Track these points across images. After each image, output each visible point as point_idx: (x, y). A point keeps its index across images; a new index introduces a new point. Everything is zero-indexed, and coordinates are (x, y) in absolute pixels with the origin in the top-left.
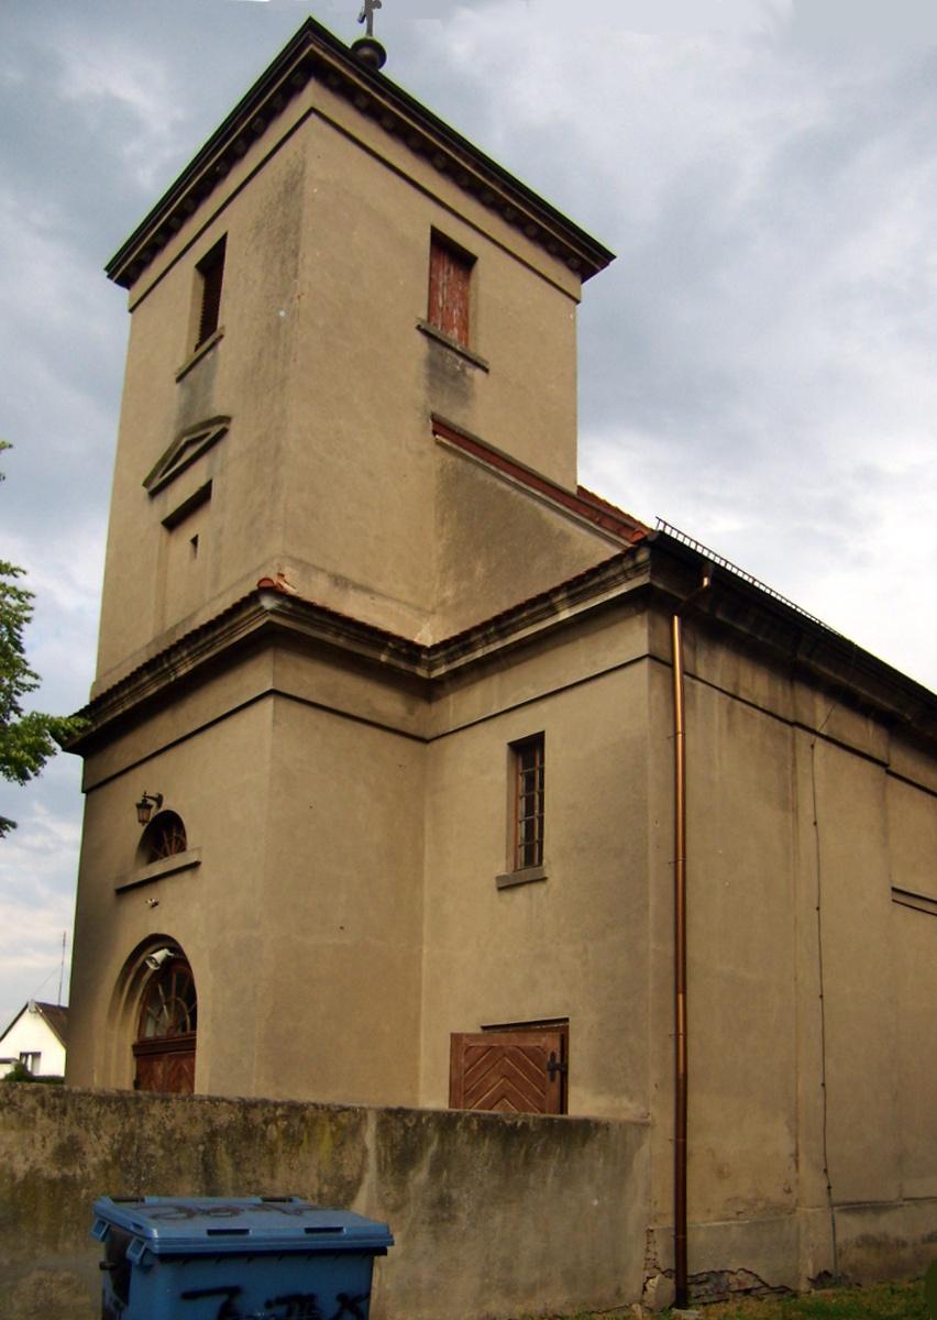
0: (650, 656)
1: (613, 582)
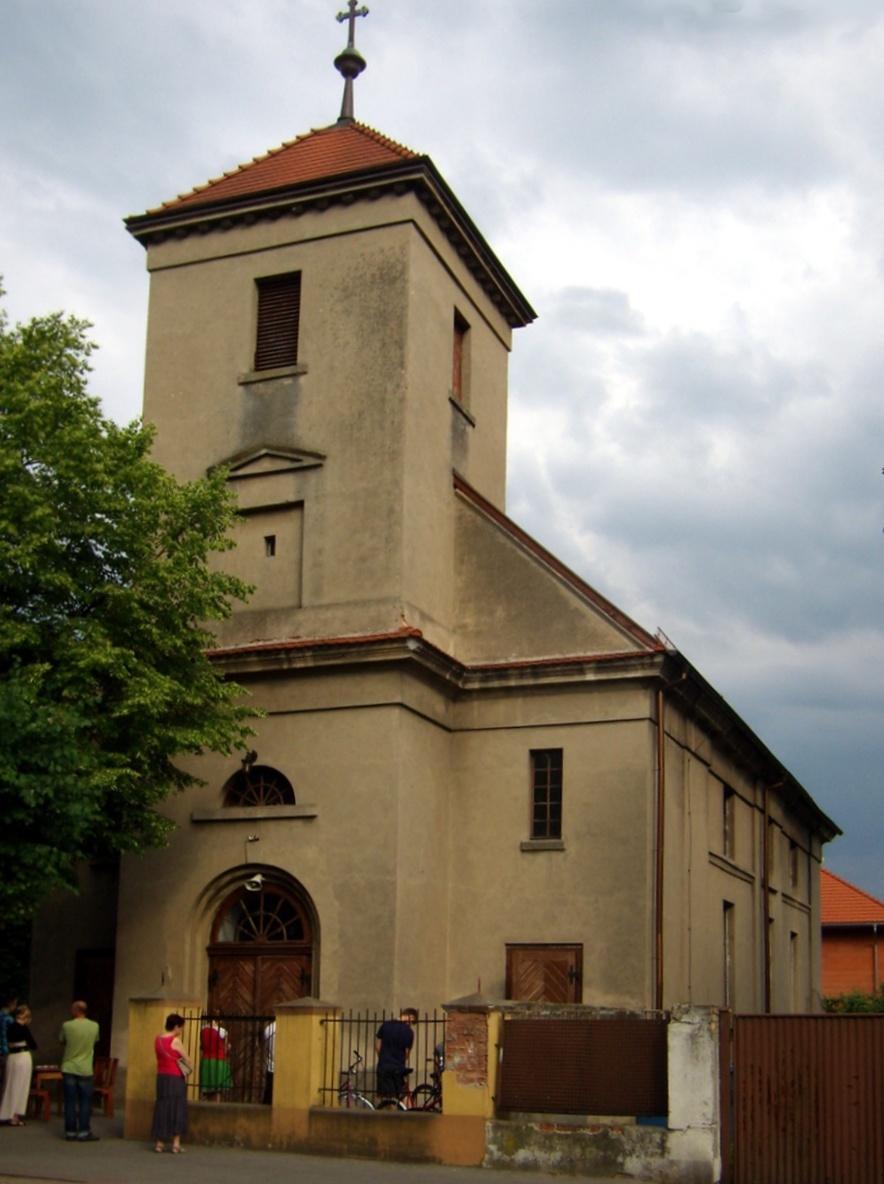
0: (650, 719)
1: (634, 668)
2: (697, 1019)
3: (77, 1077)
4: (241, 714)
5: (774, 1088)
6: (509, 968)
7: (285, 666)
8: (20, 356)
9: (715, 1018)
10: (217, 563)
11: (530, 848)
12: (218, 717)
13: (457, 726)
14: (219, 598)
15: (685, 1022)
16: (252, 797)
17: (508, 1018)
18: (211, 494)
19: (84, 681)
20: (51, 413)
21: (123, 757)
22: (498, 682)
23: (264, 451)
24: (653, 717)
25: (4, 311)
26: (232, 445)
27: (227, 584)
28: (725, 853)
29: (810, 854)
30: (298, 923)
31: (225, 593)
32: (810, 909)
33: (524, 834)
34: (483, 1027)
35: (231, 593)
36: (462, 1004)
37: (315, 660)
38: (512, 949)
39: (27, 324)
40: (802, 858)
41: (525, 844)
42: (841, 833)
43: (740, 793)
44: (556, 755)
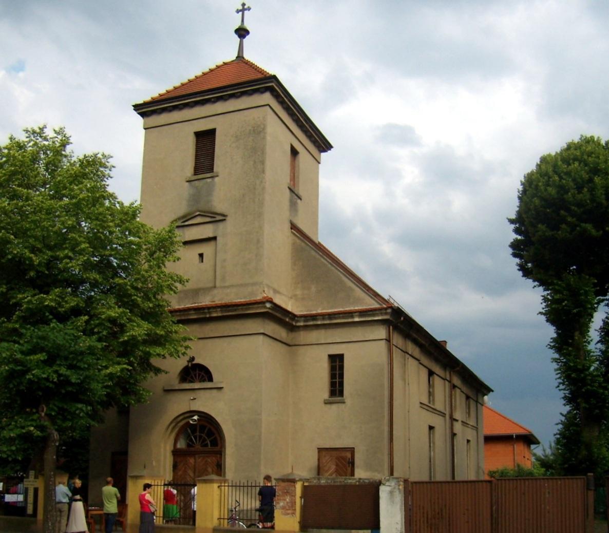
0: (386, 339)
2: (393, 484)
4: (185, 339)
5: (429, 516)
6: (319, 460)
7: (208, 316)
8: (77, 172)
9: (402, 483)
10: (170, 267)
11: (329, 402)
12: (173, 340)
13: (293, 344)
14: (172, 284)
15: (387, 486)
16: (192, 377)
17: (306, 484)
18: (168, 235)
19: (104, 325)
20: (91, 199)
21: (124, 360)
22: (313, 322)
23: (198, 213)
24: (388, 339)
25: (72, 151)
26: (182, 210)
27: (176, 278)
28: (430, 403)
29: (477, 402)
30: (215, 439)
31: (175, 282)
32: (477, 428)
33: (326, 395)
34: (293, 489)
35: (178, 282)
36: (283, 478)
37: (222, 313)
38: (320, 450)
39: (81, 157)
40: (472, 404)
41: (327, 400)
42: (493, 391)
43: (437, 373)
44: (341, 357)
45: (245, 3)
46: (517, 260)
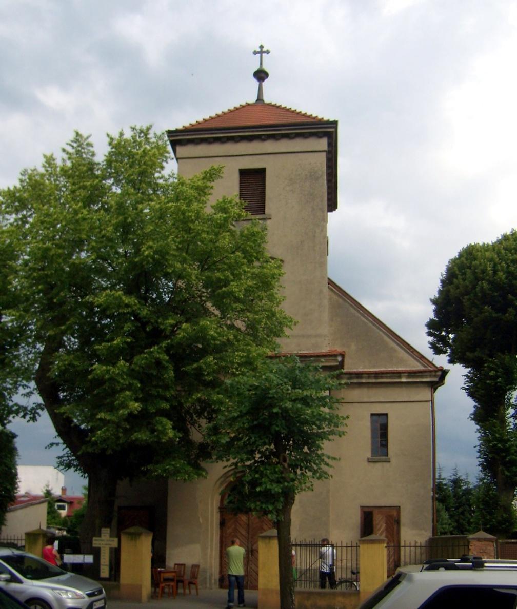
1: (426, 377)
3: (236, 576)
45: (263, 45)
46: (431, 339)
